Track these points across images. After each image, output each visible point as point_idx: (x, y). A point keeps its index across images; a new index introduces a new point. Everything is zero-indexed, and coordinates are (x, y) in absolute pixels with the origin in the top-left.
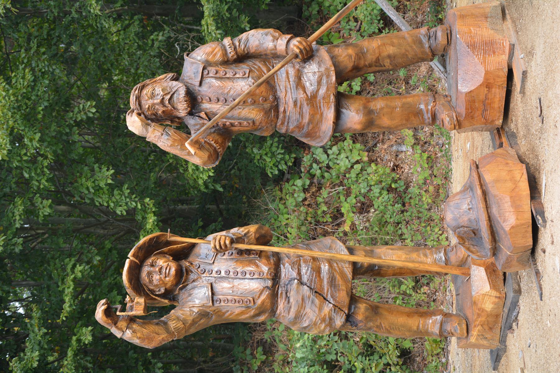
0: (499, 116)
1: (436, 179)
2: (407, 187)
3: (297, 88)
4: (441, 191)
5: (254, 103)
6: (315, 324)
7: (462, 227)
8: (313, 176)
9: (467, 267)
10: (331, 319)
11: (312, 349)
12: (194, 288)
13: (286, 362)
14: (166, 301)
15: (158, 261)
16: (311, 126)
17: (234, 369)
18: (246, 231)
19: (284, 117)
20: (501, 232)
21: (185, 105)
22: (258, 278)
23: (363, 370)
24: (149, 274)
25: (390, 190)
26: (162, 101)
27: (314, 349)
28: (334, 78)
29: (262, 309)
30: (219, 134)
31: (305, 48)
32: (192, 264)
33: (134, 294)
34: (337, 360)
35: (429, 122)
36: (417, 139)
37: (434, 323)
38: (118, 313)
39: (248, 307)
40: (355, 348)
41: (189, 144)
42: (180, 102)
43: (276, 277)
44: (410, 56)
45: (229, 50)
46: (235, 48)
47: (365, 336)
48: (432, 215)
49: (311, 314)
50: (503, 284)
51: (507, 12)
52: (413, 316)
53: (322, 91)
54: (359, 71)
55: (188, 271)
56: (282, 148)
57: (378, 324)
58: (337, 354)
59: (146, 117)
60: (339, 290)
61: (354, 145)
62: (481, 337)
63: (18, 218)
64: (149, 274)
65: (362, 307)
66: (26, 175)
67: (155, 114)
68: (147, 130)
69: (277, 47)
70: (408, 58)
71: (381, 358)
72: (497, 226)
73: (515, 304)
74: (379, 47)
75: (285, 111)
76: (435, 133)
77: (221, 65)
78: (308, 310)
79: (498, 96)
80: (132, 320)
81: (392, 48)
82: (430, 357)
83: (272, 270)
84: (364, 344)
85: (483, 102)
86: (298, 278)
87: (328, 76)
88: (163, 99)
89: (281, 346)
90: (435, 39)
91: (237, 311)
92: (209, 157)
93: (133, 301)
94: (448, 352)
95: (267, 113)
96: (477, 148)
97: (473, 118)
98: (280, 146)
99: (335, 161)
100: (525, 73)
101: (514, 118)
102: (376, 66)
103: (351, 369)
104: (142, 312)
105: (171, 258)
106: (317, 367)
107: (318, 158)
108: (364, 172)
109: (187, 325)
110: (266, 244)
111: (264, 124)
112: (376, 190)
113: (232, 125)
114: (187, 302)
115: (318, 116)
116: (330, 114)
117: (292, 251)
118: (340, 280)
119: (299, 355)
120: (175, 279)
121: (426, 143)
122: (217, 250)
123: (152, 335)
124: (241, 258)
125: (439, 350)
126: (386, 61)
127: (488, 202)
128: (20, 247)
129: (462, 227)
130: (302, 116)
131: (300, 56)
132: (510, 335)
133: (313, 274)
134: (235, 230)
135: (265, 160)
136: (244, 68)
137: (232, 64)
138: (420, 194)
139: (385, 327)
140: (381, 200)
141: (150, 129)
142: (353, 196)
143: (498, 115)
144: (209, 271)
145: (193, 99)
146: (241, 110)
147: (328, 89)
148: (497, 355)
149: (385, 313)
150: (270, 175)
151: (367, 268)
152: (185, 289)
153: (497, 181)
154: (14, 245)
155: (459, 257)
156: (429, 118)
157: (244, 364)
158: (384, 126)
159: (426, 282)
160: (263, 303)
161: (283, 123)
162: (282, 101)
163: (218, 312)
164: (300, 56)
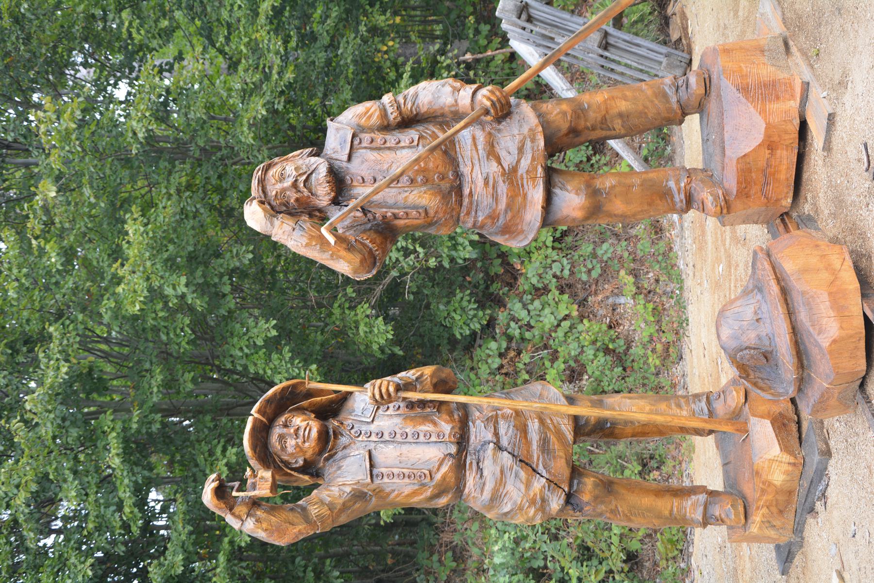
0: (787, 193)
1: (665, 335)
2: (629, 347)
3: (488, 158)
4: (671, 350)
5: (426, 181)
6: (521, 508)
7: (746, 349)
8: (510, 339)
9: (742, 420)
10: (543, 500)
11: (513, 554)
12: (344, 457)
13: (481, 571)
14: (306, 478)
15: (294, 420)
16: (510, 214)
17: (418, 579)
18: (419, 373)
19: (471, 203)
20: (814, 351)
21: (327, 189)
22: (436, 442)
23: (580, 579)
24: (282, 437)
25: (607, 351)
26: (295, 185)
27: (516, 553)
28: (542, 143)
29: (443, 488)
30: (377, 232)
31: (499, 100)
32: (342, 424)
33: (260, 467)
34: (546, 567)
35: (681, 207)
36: (638, 288)
37: (694, 506)
38: (234, 494)
39: (423, 485)
40: (568, 552)
41: (326, 228)
42: (320, 184)
43: (462, 440)
44: (650, 115)
45: (390, 110)
46: (399, 107)
47: (580, 535)
48: (662, 380)
49: (515, 492)
50: (798, 445)
51: (791, 43)
52: (663, 496)
53: (525, 163)
54: (577, 136)
55: (337, 434)
56: (475, 302)
57: (613, 508)
58: (545, 559)
59: (272, 208)
60: (554, 457)
61: (561, 296)
62: (767, 525)
63: (155, 390)
64: (282, 437)
65: (589, 482)
66: (164, 338)
67: (286, 204)
68: (272, 224)
69: (459, 101)
70: (647, 118)
71: (601, 563)
72: (806, 341)
73: (821, 473)
74: (605, 101)
75: (471, 194)
76: (662, 279)
77: (378, 131)
78: (509, 487)
79: (785, 162)
80: (255, 503)
81: (624, 103)
82: (664, 562)
83: (457, 430)
84: (579, 546)
85: (763, 171)
86: (495, 441)
87: (533, 140)
88: (296, 181)
89: (475, 551)
90: (687, 88)
91: (407, 490)
92: (361, 262)
93: (255, 476)
94: (690, 556)
95: (445, 197)
96: (737, 265)
97: (748, 196)
98: (473, 300)
99: (538, 319)
100: (831, 118)
101: (809, 196)
102: (602, 129)
103: (563, 578)
104: (269, 491)
105: (313, 416)
106: (521, 576)
107: (517, 315)
108: (574, 330)
109: (336, 511)
110: (449, 392)
111: (441, 215)
112: (590, 352)
113: (396, 217)
114: (334, 479)
115: (520, 199)
116: (537, 195)
117: (484, 401)
118: (556, 442)
119: (497, 560)
120: (317, 444)
121: (649, 292)
122: (376, 401)
123: (284, 526)
124: (412, 413)
125: (676, 552)
126: (616, 121)
127: (791, 306)
128: (158, 426)
129: (746, 349)
130: (497, 200)
131: (492, 111)
132: (810, 521)
133: (516, 435)
134: (403, 374)
135: (453, 318)
136: (413, 134)
137: (394, 130)
138: (645, 355)
139: (623, 512)
140: (596, 364)
141: (277, 222)
142: (561, 360)
143: (785, 190)
144: (366, 433)
145: (339, 182)
146: (407, 194)
147: (533, 159)
148: (789, 552)
149: (623, 491)
150: (459, 337)
151: (594, 425)
152: (332, 460)
153: (804, 270)
154: (150, 423)
155: (730, 407)
156: (681, 201)
157: (430, 573)
158: (616, 212)
159: (656, 465)
160: (444, 478)
161: (468, 213)
162: (467, 178)
163: (379, 492)
164: (492, 111)
